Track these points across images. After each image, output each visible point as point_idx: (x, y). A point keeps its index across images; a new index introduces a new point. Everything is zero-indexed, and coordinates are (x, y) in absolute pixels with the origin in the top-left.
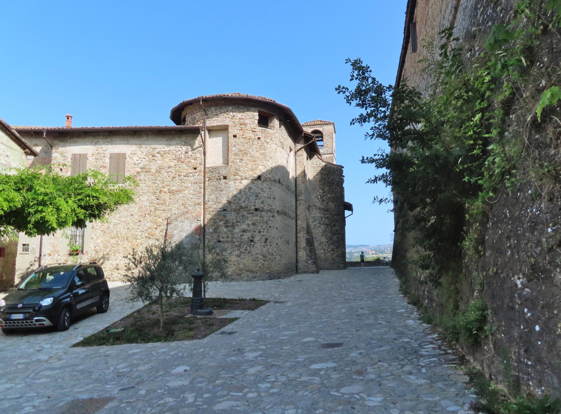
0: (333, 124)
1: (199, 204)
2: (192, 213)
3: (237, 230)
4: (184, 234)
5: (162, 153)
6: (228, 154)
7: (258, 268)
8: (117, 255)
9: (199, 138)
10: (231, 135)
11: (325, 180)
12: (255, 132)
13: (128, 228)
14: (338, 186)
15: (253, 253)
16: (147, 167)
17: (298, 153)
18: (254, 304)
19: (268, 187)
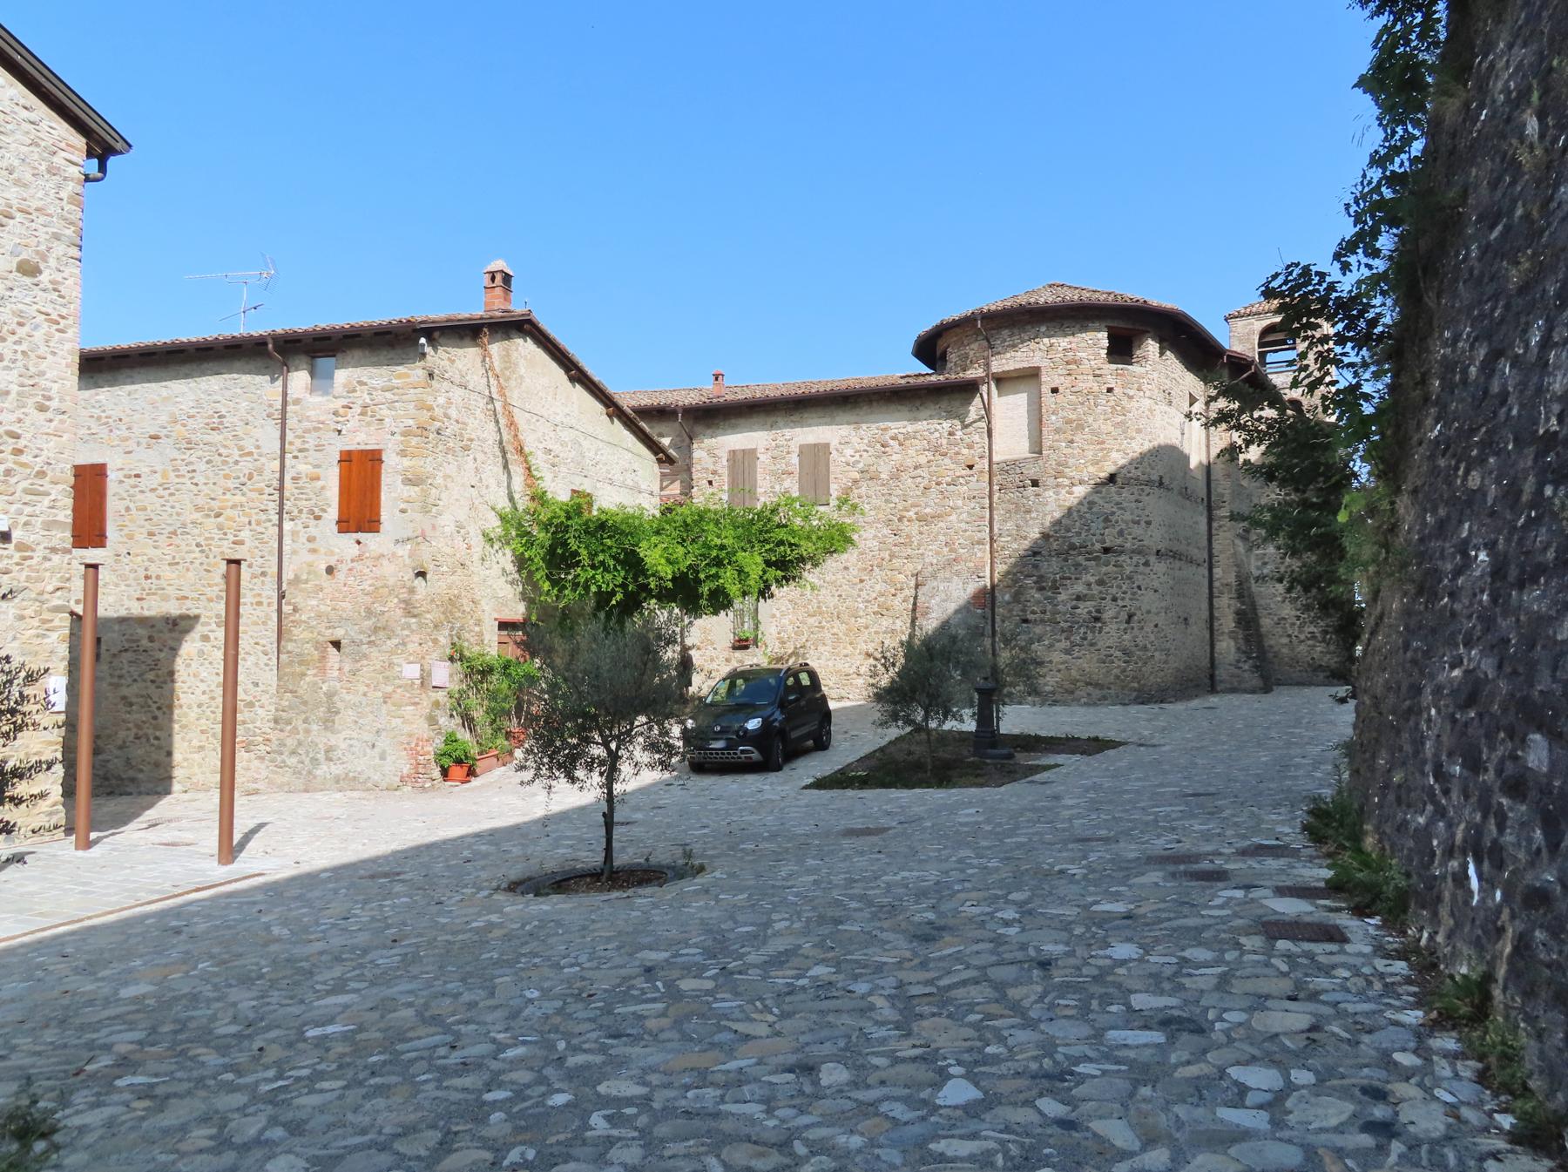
4: (952, 607)
5: (901, 437)
8: (821, 648)
9: (977, 400)
10: (1046, 389)
15: (1100, 644)
16: (873, 469)
18: (1096, 746)
19: (1133, 498)
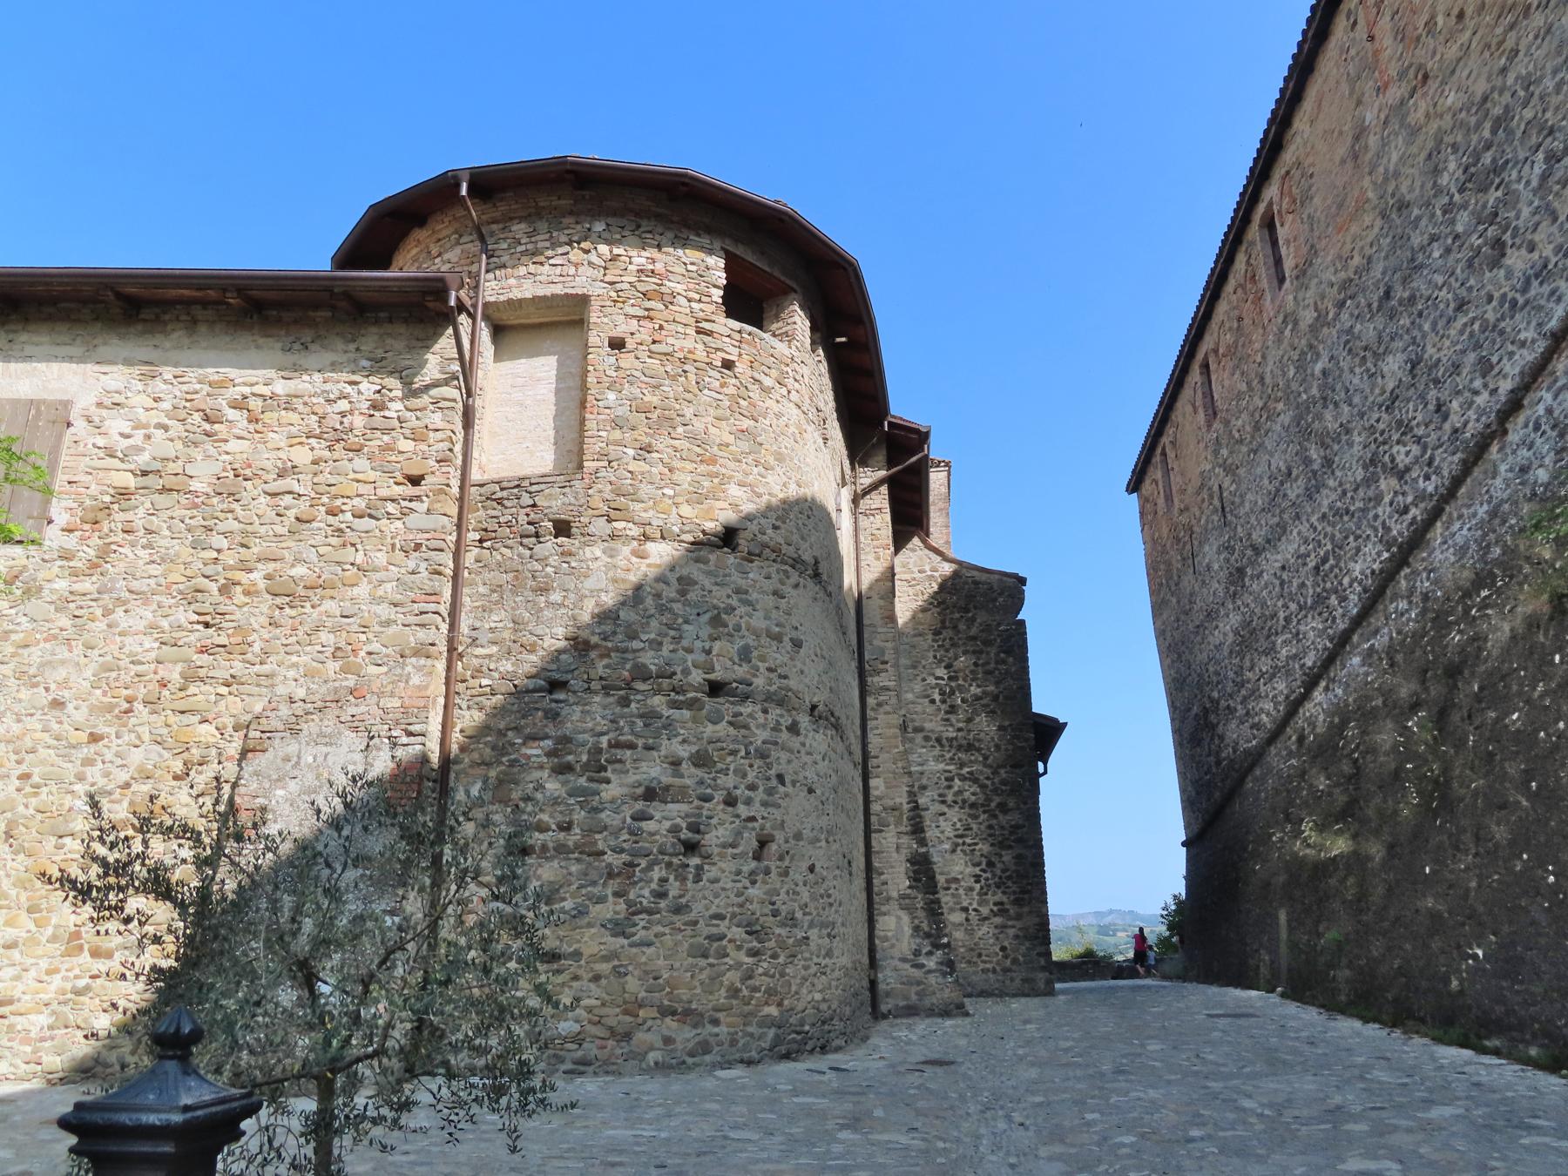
0: (947, 464)
1: (424, 651)
2: (380, 695)
3: (612, 791)
6: (582, 421)
7: (721, 996)
9: (445, 343)
11: (955, 627)
12: (709, 333)
13: (25, 777)
14: (1008, 652)
15: (698, 908)
17: (865, 503)
19: (769, 585)
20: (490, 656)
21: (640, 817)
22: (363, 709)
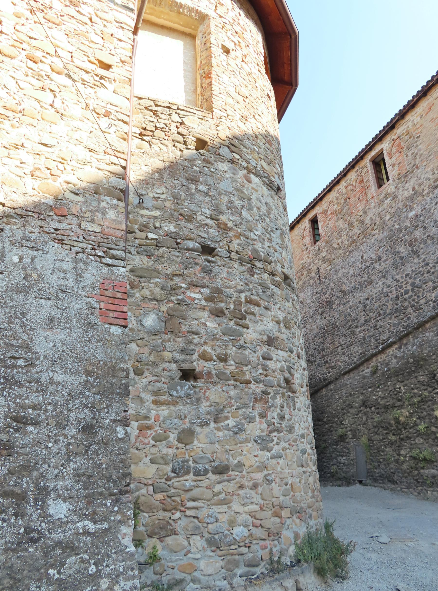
20: (155, 217)
21: (267, 358)
22: (63, 226)
